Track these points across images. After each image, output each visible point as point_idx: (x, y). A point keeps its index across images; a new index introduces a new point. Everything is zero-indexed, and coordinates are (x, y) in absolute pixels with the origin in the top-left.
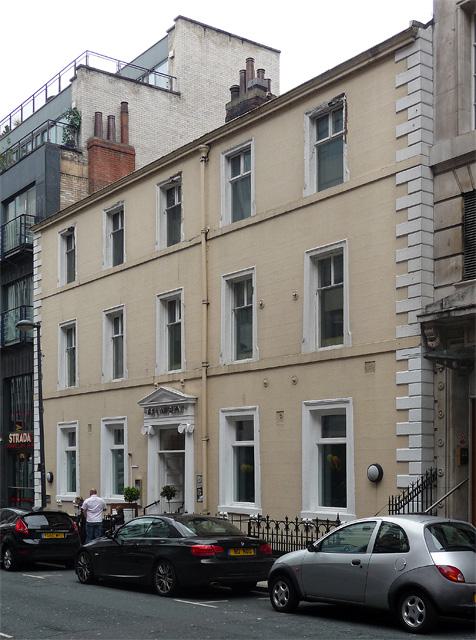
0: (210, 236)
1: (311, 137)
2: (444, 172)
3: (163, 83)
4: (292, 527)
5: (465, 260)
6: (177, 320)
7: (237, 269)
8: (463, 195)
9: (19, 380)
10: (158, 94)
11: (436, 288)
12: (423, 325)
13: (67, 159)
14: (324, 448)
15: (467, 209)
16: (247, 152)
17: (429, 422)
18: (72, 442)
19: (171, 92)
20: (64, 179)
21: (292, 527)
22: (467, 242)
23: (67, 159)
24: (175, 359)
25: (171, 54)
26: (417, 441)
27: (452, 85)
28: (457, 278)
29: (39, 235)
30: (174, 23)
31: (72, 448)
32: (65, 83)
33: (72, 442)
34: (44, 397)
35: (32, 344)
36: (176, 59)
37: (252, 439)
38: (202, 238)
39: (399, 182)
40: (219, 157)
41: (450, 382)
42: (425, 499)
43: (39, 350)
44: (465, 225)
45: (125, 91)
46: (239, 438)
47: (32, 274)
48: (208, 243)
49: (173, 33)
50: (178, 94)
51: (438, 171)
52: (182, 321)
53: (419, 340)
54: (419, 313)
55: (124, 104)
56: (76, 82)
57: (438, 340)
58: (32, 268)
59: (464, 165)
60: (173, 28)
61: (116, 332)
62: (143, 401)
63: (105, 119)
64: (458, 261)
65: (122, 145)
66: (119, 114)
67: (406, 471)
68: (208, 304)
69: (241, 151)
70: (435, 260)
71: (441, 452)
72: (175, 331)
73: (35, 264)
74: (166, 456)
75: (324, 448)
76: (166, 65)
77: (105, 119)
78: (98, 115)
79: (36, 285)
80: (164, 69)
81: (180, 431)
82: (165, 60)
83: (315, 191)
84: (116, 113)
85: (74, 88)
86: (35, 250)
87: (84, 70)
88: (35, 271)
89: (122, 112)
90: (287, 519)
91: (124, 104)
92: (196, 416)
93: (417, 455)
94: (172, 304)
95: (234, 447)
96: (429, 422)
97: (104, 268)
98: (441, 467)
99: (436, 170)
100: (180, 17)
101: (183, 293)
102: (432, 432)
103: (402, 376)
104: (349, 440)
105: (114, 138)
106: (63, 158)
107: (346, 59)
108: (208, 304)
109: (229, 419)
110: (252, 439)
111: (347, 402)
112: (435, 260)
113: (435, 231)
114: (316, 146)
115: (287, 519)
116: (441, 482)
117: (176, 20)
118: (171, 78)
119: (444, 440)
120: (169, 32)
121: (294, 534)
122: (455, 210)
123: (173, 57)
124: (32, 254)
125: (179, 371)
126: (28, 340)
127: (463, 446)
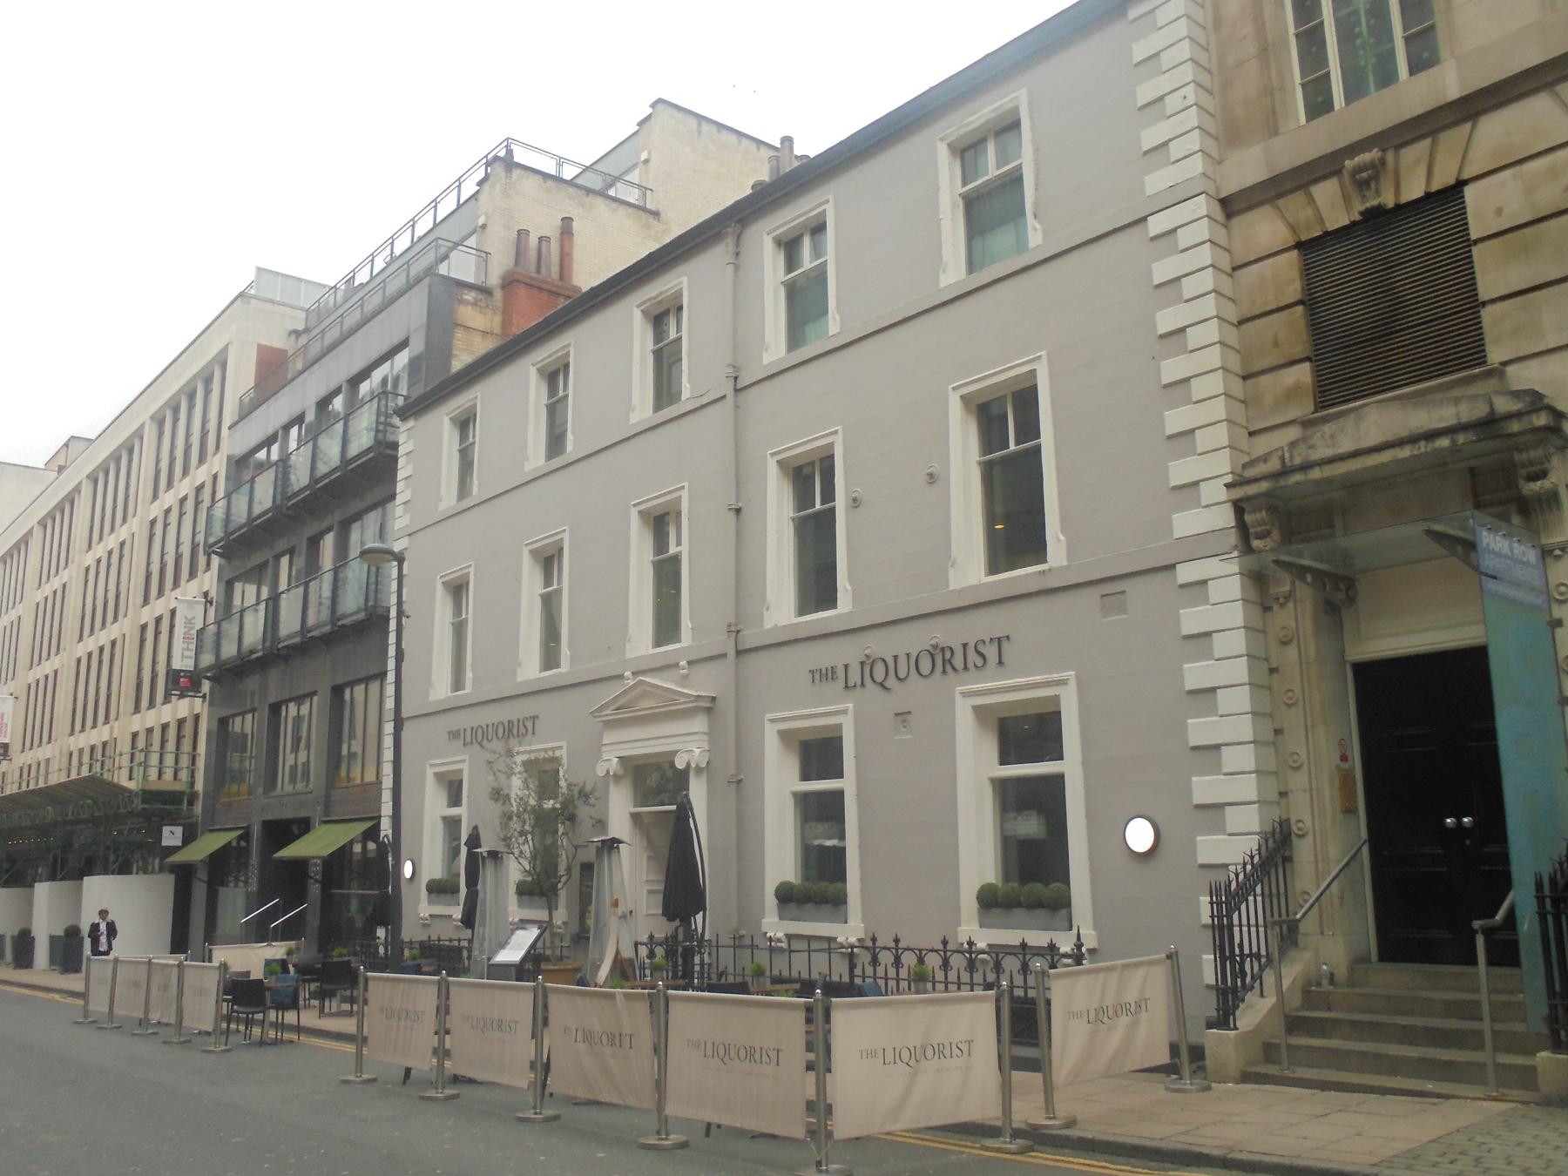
0: (741, 384)
1: (952, 179)
2: (1251, 208)
3: (633, 196)
4: (886, 958)
5: (1318, 373)
6: (673, 550)
7: (801, 444)
8: (1299, 245)
9: (359, 690)
10: (622, 210)
11: (1251, 434)
12: (1239, 507)
13: (467, 303)
14: (803, 800)
15: (1307, 272)
16: (818, 229)
17: (1263, 715)
18: (455, 800)
19: (643, 209)
20: (459, 334)
21: (886, 958)
22: (1315, 326)
23: (467, 303)
24: (667, 626)
25: (644, 156)
26: (1243, 758)
27: (1251, 49)
28: (1305, 408)
29: (411, 423)
30: (651, 110)
31: (454, 811)
32: (469, 188)
33: (455, 800)
34: (404, 715)
35: (387, 619)
36: (652, 164)
37: (841, 775)
38: (728, 389)
39: (1153, 231)
40: (763, 239)
41: (1308, 627)
42: (1267, 891)
43: (400, 603)
44: (1309, 302)
45: (567, 205)
46: (805, 777)
47: (393, 496)
48: (742, 395)
49: (646, 126)
50: (656, 214)
51: (1236, 208)
52: (684, 549)
53: (1233, 538)
54: (1229, 479)
55: (567, 222)
56: (486, 186)
57: (1276, 534)
58: (394, 481)
59: (1298, 188)
60: (648, 118)
61: (548, 581)
62: (600, 709)
63: (533, 241)
64: (1303, 374)
65: (560, 283)
66: (558, 236)
67: (1220, 828)
68: (738, 511)
69: (804, 225)
70: (1245, 378)
71: (1298, 781)
72: (667, 574)
73: (401, 475)
74: (646, 820)
75: (803, 800)
76: (636, 172)
77: (533, 241)
78: (522, 234)
79: (399, 511)
80: (634, 177)
81: (680, 764)
82: (634, 166)
83: (964, 276)
84: (553, 233)
85: (484, 197)
86: (402, 450)
87: (503, 164)
88: (400, 487)
89: (562, 234)
90: (897, 941)
91: (567, 222)
92: (711, 734)
93: (1247, 788)
94: (660, 523)
95: (993, 781)
96: (1263, 715)
97: (528, 467)
98: (1301, 812)
99: (1231, 206)
100: (660, 101)
101: (685, 495)
102: (1270, 736)
103: (1193, 619)
104: (847, 784)
105: (549, 269)
106: (462, 302)
107: (1012, 39)
108: (738, 511)
109: (783, 735)
110: (841, 775)
111: (1061, 683)
112: (1245, 378)
113: (1241, 323)
114: (965, 197)
115: (897, 941)
116: (1303, 851)
117: (653, 105)
118: (644, 189)
119: (1303, 754)
120: (641, 124)
121: (892, 972)
122: (1285, 276)
123: (646, 161)
124: (396, 459)
125: (677, 646)
126: (380, 611)
127: (1345, 766)
